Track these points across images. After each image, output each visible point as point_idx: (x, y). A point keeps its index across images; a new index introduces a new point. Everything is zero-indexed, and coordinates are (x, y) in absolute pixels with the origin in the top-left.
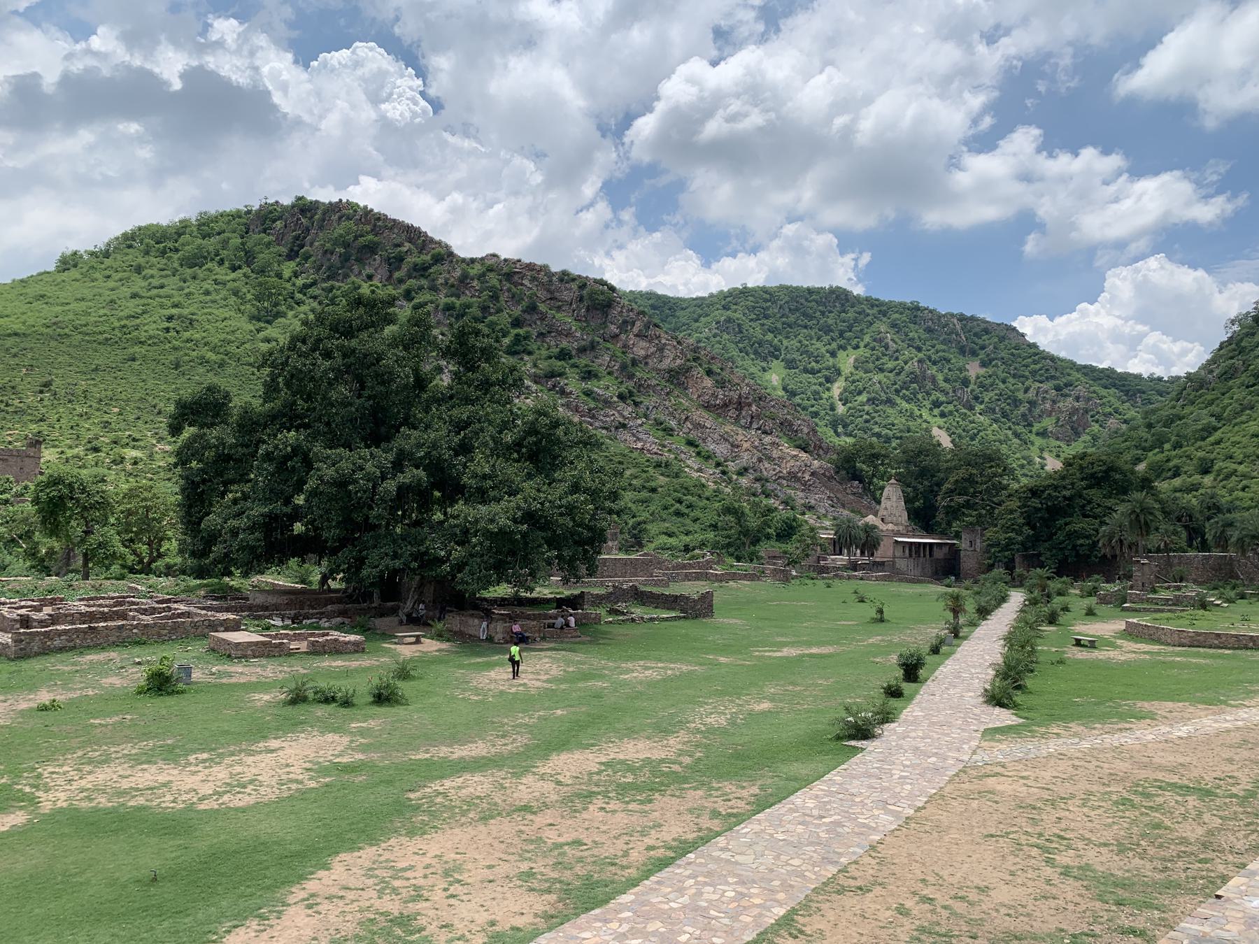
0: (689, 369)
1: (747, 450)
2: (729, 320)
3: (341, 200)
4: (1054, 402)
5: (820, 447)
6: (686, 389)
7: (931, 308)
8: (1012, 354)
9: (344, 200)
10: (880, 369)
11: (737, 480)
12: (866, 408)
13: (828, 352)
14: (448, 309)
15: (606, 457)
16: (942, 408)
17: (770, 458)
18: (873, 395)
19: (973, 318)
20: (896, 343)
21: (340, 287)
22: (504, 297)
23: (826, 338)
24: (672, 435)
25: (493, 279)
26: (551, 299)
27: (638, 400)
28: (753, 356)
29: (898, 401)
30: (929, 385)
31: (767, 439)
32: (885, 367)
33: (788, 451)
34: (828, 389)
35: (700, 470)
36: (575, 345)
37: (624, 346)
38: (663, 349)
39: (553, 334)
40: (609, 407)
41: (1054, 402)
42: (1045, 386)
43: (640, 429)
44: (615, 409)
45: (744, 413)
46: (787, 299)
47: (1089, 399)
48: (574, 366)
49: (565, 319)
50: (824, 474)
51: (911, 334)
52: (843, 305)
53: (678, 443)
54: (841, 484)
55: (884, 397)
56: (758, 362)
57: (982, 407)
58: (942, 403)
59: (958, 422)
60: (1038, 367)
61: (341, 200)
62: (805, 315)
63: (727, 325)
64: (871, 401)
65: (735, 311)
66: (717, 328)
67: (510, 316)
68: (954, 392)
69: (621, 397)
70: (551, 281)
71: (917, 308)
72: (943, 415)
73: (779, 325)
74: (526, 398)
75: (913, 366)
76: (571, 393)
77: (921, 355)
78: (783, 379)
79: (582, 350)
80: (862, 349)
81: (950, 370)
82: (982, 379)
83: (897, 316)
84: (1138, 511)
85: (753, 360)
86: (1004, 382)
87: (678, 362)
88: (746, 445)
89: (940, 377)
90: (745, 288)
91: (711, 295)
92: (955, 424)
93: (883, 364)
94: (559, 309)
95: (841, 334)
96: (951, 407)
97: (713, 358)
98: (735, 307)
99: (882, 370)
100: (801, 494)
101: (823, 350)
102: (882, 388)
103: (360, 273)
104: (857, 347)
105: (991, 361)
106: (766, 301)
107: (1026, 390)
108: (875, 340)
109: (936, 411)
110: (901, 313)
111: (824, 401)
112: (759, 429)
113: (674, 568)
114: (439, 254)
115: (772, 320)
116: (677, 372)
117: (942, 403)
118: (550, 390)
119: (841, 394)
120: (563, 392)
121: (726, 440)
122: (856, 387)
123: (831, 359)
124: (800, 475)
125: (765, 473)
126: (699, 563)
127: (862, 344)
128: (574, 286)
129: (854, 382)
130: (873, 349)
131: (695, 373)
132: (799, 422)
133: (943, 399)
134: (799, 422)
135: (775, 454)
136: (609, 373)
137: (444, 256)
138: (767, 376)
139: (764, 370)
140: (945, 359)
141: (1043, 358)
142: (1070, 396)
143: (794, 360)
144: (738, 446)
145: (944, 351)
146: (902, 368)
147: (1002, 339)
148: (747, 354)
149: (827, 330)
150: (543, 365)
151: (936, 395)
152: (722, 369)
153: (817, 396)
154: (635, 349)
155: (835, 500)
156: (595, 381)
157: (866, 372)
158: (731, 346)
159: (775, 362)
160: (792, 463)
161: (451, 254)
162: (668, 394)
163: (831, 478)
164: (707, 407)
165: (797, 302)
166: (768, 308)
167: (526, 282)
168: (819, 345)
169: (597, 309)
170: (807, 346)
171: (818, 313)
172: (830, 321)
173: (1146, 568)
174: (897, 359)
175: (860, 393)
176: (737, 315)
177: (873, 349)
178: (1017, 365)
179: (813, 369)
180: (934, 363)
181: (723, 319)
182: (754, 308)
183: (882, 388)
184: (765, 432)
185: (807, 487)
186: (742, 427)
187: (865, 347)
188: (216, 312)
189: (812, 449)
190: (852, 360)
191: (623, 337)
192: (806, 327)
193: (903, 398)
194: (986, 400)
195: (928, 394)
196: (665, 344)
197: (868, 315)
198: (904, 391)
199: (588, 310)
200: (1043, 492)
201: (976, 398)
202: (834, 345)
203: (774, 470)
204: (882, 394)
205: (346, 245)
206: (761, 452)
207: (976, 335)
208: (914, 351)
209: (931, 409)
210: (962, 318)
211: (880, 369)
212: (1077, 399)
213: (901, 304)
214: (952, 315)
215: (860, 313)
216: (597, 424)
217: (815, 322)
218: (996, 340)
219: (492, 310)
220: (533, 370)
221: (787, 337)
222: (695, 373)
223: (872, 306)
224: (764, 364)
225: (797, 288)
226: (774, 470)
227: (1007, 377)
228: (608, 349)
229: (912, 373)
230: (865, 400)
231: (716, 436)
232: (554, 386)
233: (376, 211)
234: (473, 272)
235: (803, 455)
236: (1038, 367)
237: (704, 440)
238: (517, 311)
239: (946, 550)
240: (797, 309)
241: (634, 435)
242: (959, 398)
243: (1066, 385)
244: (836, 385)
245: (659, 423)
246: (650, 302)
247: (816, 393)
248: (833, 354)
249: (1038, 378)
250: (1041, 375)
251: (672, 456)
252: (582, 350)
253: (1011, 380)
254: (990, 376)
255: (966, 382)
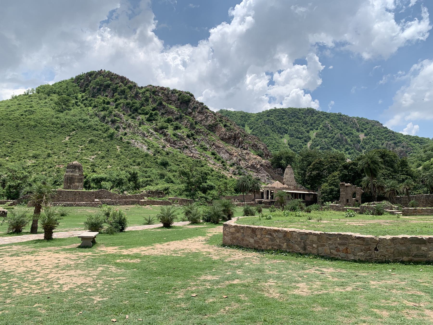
0: (216, 125)
1: (236, 156)
2: (269, 120)
3: (101, 70)
4: (393, 148)
5: (268, 155)
6: (215, 133)
7: (346, 115)
8: (377, 131)
9: (103, 70)
10: (326, 137)
11: (229, 168)
12: (319, 151)
13: (306, 131)
14: (128, 105)
15: (175, 159)
16: (349, 151)
17: (244, 159)
18: (322, 146)
19: (362, 118)
20: (332, 127)
21: (94, 100)
22: (150, 100)
23: (305, 126)
24: (206, 151)
25: (148, 94)
26: (168, 100)
27: (195, 137)
28: (277, 133)
29: (332, 148)
30: (344, 143)
31: (245, 152)
32: (328, 136)
33: (253, 156)
34: (306, 145)
35: (214, 164)
36: (175, 117)
37: (194, 117)
38: (208, 117)
39: (167, 113)
40: (182, 140)
41: (393, 148)
42: (390, 143)
43: (193, 148)
44: (184, 141)
45: (236, 141)
46: (291, 112)
47: (408, 147)
48: (172, 125)
49: (172, 107)
50: (266, 166)
51: (338, 124)
52: (312, 114)
53: (208, 154)
54: (273, 170)
55: (326, 147)
56: (279, 135)
57: (365, 150)
58: (349, 149)
59: (355, 156)
60: (387, 135)
61: (101, 70)
62: (298, 118)
63: (267, 122)
64: (321, 148)
65: (271, 117)
66: (264, 123)
67: (152, 107)
68: (354, 145)
69: (188, 136)
70: (168, 93)
71: (341, 115)
72: (349, 154)
73: (288, 122)
74: (150, 137)
75: (338, 135)
76: (168, 135)
77: (341, 132)
78: (288, 141)
79: (177, 119)
80: (319, 130)
81: (353, 137)
82: (365, 140)
83: (333, 118)
84: (369, 163)
85: (277, 134)
86: (374, 141)
87: (213, 122)
88: (235, 154)
89: (349, 140)
90: (276, 109)
91: (263, 112)
92: (354, 157)
93: (327, 135)
94: (170, 104)
95: (311, 125)
96: (353, 151)
97: (228, 121)
98: (271, 115)
99: (326, 137)
100: (255, 174)
101: (304, 130)
102: (326, 144)
103: (103, 95)
104: (317, 129)
105: (369, 133)
106: (283, 113)
107: (382, 144)
108: (324, 127)
109: (347, 152)
110: (335, 117)
111: (304, 149)
112: (242, 147)
113: (119, 198)
114: (131, 86)
115: (285, 120)
116: (212, 126)
117: (349, 149)
118: (161, 134)
119: (310, 146)
120: (165, 135)
121: (228, 152)
122: (316, 143)
123: (307, 134)
124: (255, 166)
125: (241, 165)
126: (136, 196)
127: (319, 128)
128: (177, 95)
129: (315, 141)
130: (323, 130)
131: (219, 126)
132: (260, 145)
133: (349, 147)
134: (260, 145)
135: (247, 157)
136: (186, 127)
137: (133, 86)
138: (282, 140)
139: (281, 138)
140: (351, 133)
141: (389, 132)
142: (400, 146)
143: (293, 134)
144: (232, 155)
145: (351, 130)
146: (334, 136)
147: (373, 126)
148: (275, 132)
149: (306, 123)
150: (159, 124)
151: (347, 146)
152: (231, 125)
153: (301, 147)
154: (197, 118)
155: (270, 176)
156: (179, 130)
157: (320, 138)
158: (268, 129)
159: (286, 135)
160: (253, 161)
161: (135, 86)
162: (207, 135)
163: (268, 168)
164: (222, 139)
165: (295, 113)
166: (284, 116)
167: (160, 94)
168: (302, 128)
169: (184, 103)
170: (298, 129)
171: (303, 117)
172: (307, 120)
173: (349, 189)
174: (332, 133)
175: (317, 146)
176: (272, 118)
177: (323, 130)
178: (379, 135)
179: (300, 137)
180: (347, 135)
181: (266, 120)
182: (279, 116)
183: (326, 144)
184: (244, 149)
185: (258, 171)
186: (235, 147)
187: (320, 129)
188: (43, 109)
189: (264, 156)
190: (315, 134)
191: (193, 113)
192: (298, 122)
193: (334, 147)
194: (367, 148)
195: (344, 146)
196: (209, 115)
197: (322, 118)
198: (335, 145)
199: (181, 103)
200: (349, 166)
201: (363, 147)
202: (308, 129)
203: (245, 164)
204: (326, 146)
205: (101, 85)
206: (241, 157)
207: (363, 124)
208: (339, 130)
209: (345, 152)
210: (358, 119)
211: (326, 137)
212: (403, 147)
213: (334, 114)
214: (354, 118)
215: (319, 117)
216: (176, 147)
217: (301, 120)
218: (371, 126)
219: (145, 105)
220: (155, 126)
221: (291, 126)
222: (219, 126)
223: (324, 115)
224: (281, 136)
225: (295, 109)
226: (245, 164)
227: (375, 140)
228: (187, 118)
229: (337, 138)
230: (319, 148)
231: (224, 151)
232: (162, 132)
233: (112, 72)
234: (140, 91)
235: (259, 158)
236: (387, 135)
237: (219, 153)
238: (155, 105)
239: (312, 197)
240: (295, 116)
241: (190, 151)
242: (356, 147)
243: (398, 142)
244: (309, 143)
245: (202, 146)
246: (241, 115)
247: (301, 146)
248: (308, 132)
249: (387, 140)
250: (389, 139)
251: (204, 159)
252: (177, 119)
253: (377, 140)
254: (368, 139)
255: (359, 142)
